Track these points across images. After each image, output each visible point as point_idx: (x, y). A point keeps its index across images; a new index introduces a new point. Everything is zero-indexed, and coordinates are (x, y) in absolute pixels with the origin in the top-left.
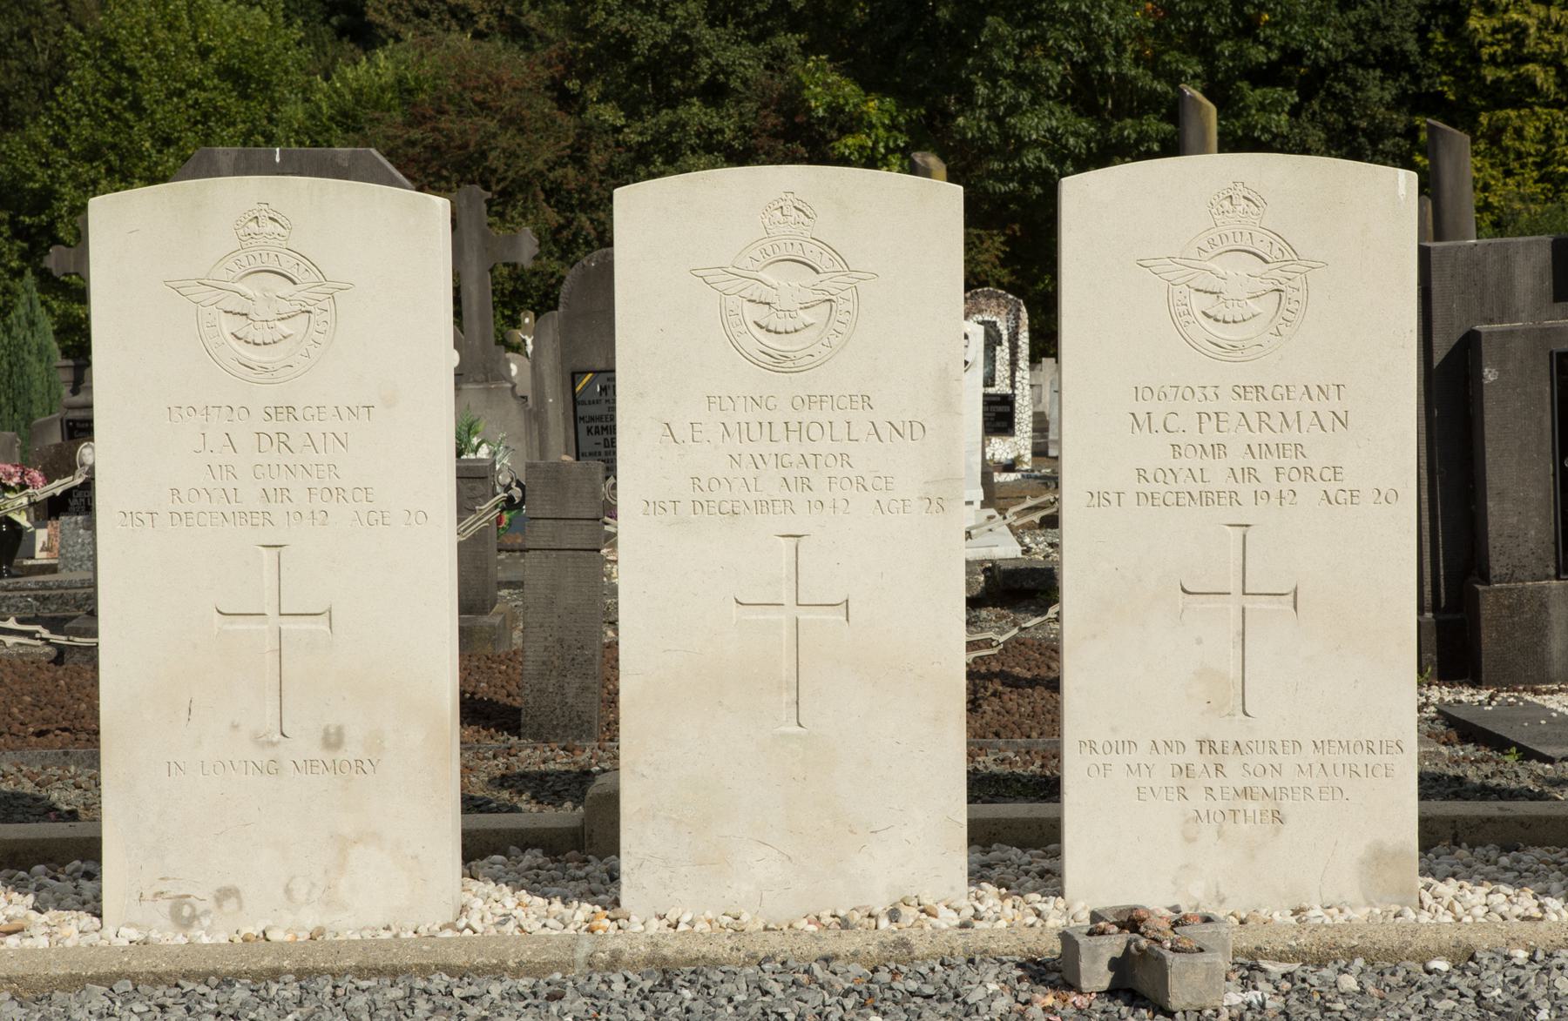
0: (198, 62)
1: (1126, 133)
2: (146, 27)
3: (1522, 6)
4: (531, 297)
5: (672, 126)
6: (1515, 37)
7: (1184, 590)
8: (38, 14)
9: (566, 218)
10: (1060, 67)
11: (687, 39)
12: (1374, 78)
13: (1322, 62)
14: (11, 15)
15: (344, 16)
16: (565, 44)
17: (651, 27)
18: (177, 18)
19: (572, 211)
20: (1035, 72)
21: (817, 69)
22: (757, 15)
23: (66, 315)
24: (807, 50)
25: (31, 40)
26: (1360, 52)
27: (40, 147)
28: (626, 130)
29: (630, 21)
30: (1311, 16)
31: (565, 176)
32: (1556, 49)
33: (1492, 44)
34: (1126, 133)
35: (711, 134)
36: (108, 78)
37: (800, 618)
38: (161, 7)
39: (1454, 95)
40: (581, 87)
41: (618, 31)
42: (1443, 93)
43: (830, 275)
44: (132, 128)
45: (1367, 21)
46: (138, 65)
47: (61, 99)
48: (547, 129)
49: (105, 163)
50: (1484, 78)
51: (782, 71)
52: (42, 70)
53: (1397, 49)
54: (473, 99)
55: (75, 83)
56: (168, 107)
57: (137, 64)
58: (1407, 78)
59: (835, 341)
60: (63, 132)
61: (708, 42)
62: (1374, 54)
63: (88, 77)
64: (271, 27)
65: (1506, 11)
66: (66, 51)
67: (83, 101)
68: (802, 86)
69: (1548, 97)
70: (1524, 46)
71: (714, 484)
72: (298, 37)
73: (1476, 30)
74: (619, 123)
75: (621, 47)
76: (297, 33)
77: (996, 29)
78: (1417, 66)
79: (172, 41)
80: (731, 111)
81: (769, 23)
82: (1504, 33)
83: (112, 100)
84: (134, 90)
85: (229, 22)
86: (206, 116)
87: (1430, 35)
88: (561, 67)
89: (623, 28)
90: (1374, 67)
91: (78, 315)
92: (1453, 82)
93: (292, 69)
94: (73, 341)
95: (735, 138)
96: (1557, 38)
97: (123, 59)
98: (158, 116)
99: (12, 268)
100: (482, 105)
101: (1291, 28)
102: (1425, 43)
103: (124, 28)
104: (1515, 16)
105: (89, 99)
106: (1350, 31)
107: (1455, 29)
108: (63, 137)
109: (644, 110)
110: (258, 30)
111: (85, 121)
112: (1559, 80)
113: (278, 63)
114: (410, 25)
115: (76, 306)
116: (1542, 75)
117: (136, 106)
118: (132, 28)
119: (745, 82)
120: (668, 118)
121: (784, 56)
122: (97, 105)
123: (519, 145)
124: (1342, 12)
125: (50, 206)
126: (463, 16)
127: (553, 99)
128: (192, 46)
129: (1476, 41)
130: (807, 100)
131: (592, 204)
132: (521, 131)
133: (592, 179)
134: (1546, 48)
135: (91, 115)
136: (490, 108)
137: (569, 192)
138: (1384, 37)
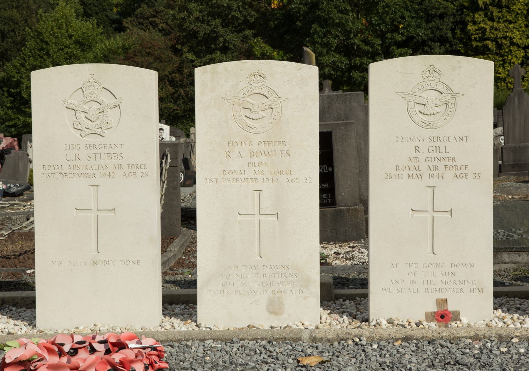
0: (68, 39)
1: (357, 62)
2: (51, 28)
3: (485, 22)
4: (164, 116)
6: (482, 32)
8: (17, 23)
9: (176, 90)
10: (336, 41)
11: (215, 32)
13: (420, 40)
14: (9, 24)
15: (117, 25)
16: (176, 33)
17: (204, 28)
18: (61, 25)
19: (178, 88)
20: (328, 42)
21: (257, 42)
22: (239, 24)
23: (24, 121)
24: (255, 35)
25: (15, 33)
26: (433, 37)
27: (17, 67)
28: (196, 61)
29: (197, 26)
30: (416, 25)
31: (175, 76)
33: (475, 34)
34: (357, 62)
36: (39, 44)
38: (57, 22)
39: (464, 51)
40: (182, 47)
41: (193, 29)
42: (460, 50)
45: (435, 27)
46: (48, 40)
47: (23, 51)
48: (170, 61)
50: (473, 45)
51: (246, 42)
52: (18, 42)
53: (444, 36)
55: (28, 46)
58: (449, 45)
59: (448, 118)
60: (24, 62)
61: (222, 33)
62: (437, 38)
63: (33, 44)
64: (92, 28)
65: (480, 23)
66: (26, 36)
67: (31, 52)
68: (252, 47)
69: (493, 51)
70: (485, 35)
72: (101, 32)
73: (470, 30)
74: (195, 58)
75: (194, 34)
76: (100, 30)
77: (316, 29)
78: (452, 41)
79: (60, 33)
80: (230, 56)
81: (242, 27)
82: (479, 31)
83: (40, 52)
85: (79, 26)
86: (70, 57)
87: (456, 31)
88: (175, 41)
89: (195, 28)
90: (437, 42)
91: (28, 122)
92: (463, 47)
93: (99, 42)
94: (27, 130)
96: (496, 32)
99: (8, 106)
100: (148, 53)
101: (410, 29)
102: (454, 34)
103: (44, 28)
104: (482, 25)
105: (33, 51)
106: (430, 30)
107: (464, 30)
108: (24, 64)
109: (202, 55)
110: (88, 29)
111: (31, 58)
112: (497, 46)
115: (28, 119)
116: (491, 44)
117: (47, 54)
118: (47, 28)
119: (234, 45)
120: (209, 58)
121: (247, 37)
122: (35, 53)
123: (160, 66)
124: (427, 24)
125: (20, 86)
126: (154, 24)
127: (171, 51)
128: (66, 34)
129: (470, 33)
131: (184, 86)
132: (161, 61)
133: (184, 77)
134: (492, 36)
135: (33, 56)
136: (151, 54)
137: (177, 82)
138: (440, 32)
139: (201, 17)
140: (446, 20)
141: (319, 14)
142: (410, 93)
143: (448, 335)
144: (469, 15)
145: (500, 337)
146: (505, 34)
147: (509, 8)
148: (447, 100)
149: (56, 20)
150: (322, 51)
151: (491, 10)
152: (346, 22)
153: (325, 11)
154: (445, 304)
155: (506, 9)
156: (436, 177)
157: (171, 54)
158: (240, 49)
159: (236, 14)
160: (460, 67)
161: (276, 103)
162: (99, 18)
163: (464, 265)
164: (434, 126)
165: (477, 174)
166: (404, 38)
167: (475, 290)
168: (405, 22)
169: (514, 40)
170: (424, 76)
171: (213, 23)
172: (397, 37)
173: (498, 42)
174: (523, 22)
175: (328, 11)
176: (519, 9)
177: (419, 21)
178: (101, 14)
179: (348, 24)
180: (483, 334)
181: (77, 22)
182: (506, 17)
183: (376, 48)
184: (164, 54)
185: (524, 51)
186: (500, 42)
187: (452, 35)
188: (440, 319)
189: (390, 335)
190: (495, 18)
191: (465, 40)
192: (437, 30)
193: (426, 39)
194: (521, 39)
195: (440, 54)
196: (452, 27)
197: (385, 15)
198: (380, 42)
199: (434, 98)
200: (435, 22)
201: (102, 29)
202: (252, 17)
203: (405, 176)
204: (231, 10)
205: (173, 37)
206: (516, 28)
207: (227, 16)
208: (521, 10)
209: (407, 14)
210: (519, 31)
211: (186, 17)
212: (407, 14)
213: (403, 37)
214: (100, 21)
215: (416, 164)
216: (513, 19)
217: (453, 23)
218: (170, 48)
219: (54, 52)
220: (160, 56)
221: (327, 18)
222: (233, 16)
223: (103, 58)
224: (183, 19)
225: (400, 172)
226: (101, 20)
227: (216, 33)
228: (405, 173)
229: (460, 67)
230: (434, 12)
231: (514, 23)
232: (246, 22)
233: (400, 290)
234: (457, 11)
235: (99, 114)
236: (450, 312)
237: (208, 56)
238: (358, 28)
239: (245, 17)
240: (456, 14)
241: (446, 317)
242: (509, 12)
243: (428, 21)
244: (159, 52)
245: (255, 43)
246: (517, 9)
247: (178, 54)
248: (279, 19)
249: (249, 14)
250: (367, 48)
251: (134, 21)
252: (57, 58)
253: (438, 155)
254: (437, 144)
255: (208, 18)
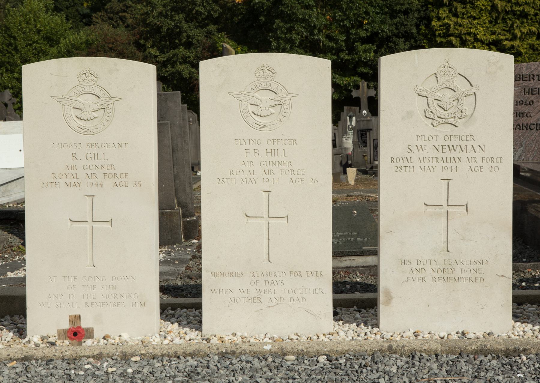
0: (37, 34)
5: (174, 55)
6: (447, 28)
7: (425, 204)
11: (178, 27)
12: (402, 42)
13: (385, 36)
16: (140, 28)
17: (167, 23)
18: (30, 20)
22: (202, 19)
24: (219, 30)
26: (398, 33)
28: (159, 57)
29: (160, 21)
30: (381, 21)
32: (460, 32)
33: (439, 30)
35: (186, 58)
36: (7, 40)
37: (94, 226)
40: (145, 42)
41: (156, 24)
43: (104, 99)
44: (14, 56)
45: (399, 23)
46: (16, 35)
49: (5, 68)
50: (437, 41)
53: (409, 32)
54: (108, 47)
56: (26, 49)
57: (16, 35)
59: (106, 123)
62: (402, 33)
65: (444, 19)
70: (449, 31)
71: (238, 173)
73: (434, 26)
74: (158, 54)
75: (158, 29)
77: (279, 24)
78: (416, 37)
81: (206, 21)
82: (443, 27)
83: (8, 47)
84: (15, 43)
86: (39, 52)
87: (420, 27)
89: (158, 23)
90: (402, 38)
92: (428, 42)
95: (194, 59)
96: (460, 29)
97: (12, 33)
98: (23, 52)
100: (111, 49)
102: (419, 30)
103: (12, 23)
104: (447, 21)
106: (394, 26)
107: (428, 25)
109: (166, 50)
112: (461, 42)
113: (63, 35)
114: (107, 22)
116: (455, 40)
117: (16, 49)
118: (15, 23)
119: (198, 41)
121: (211, 32)
124: (391, 19)
127: (135, 46)
128: (34, 30)
130: (218, 47)
134: (456, 31)
136: (114, 50)
138: (405, 28)
139: (164, 12)
140: (411, 16)
141: (282, 9)
142: (243, 93)
143: (70, 354)
144: (433, 11)
145: (124, 355)
146: (469, 30)
147: (473, 4)
148: (282, 101)
149: (24, 15)
150: (285, 46)
151: (455, 6)
152: (310, 18)
153: (288, 7)
154: (78, 321)
155: (471, 5)
156: (94, 186)
157: (134, 49)
158: (204, 45)
159: (200, 9)
160: (118, 70)
161: (286, 99)
162: (69, 13)
163: (125, 277)
164: (92, 132)
165: (137, 182)
166: (368, 34)
167: (137, 303)
168: (369, 17)
169: (478, 36)
170: (79, 79)
171: (177, 18)
172: (361, 33)
173: (463, 38)
174: (487, 18)
175: (291, 6)
176: (483, 5)
177: (383, 16)
178: (72, 9)
179: (312, 20)
180: (108, 352)
181: (46, 16)
182: (470, 13)
183: (340, 45)
184: (127, 49)
185: (488, 47)
186: (464, 39)
187: (417, 31)
188: (73, 337)
189: (9, 355)
190: (459, 14)
191: (429, 36)
192: (401, 26)
193: (391, 35)
194: (485, 35)
195: (405, 51)
196: (416, 23)
197: (349, 11)
198: (344, 38)
199: (91, 102)
200: (400, 18)
201: (71, 24)
202: (216, 12)
203: (62, 184)
204: (196, 5)
205: (136, 32)
206: (480, 24)
207: (191, 10)
208: (485, 6)
209: (371, 9)
210: (483, 27)
211: (149, 12)
212: (371, 9)
213: (368, 33)
214: (70, 15)
215: (74, 172)
216: (478, 15)
217: (417, 18)
218: (133, 43)
219: (23, 48)
220: (123, 51)
221: (290, 13)
222: (197, 11)
223: (67, 53)
224: (147, 14)
225: (57, 180)
226: (71, 14)
227: (180, 29)
228: (62, 181)
229: (118, 70)
230: (398, 8)
231: (478, 19)
232: (209, 17)
233: (59, 304)
234: (422, 7)
235: (453, 102)
236: (83, 329)
237: (171, 51)
238: (322, 23)
239: (209, 12)
240: (421, 9)
241: (79, 335)
242: (473, 8)
243: (392, 17)
244: (122, 47)
245: (219, 38)
246: (481, 5)
247: (141, 50)
248: (243, 14)
249: (213, 9)
250: (331, 44)
251: (104, 16)
252: (25, 53)
253: (97, 163)
254: (95, 150)
255: (171, 12)
